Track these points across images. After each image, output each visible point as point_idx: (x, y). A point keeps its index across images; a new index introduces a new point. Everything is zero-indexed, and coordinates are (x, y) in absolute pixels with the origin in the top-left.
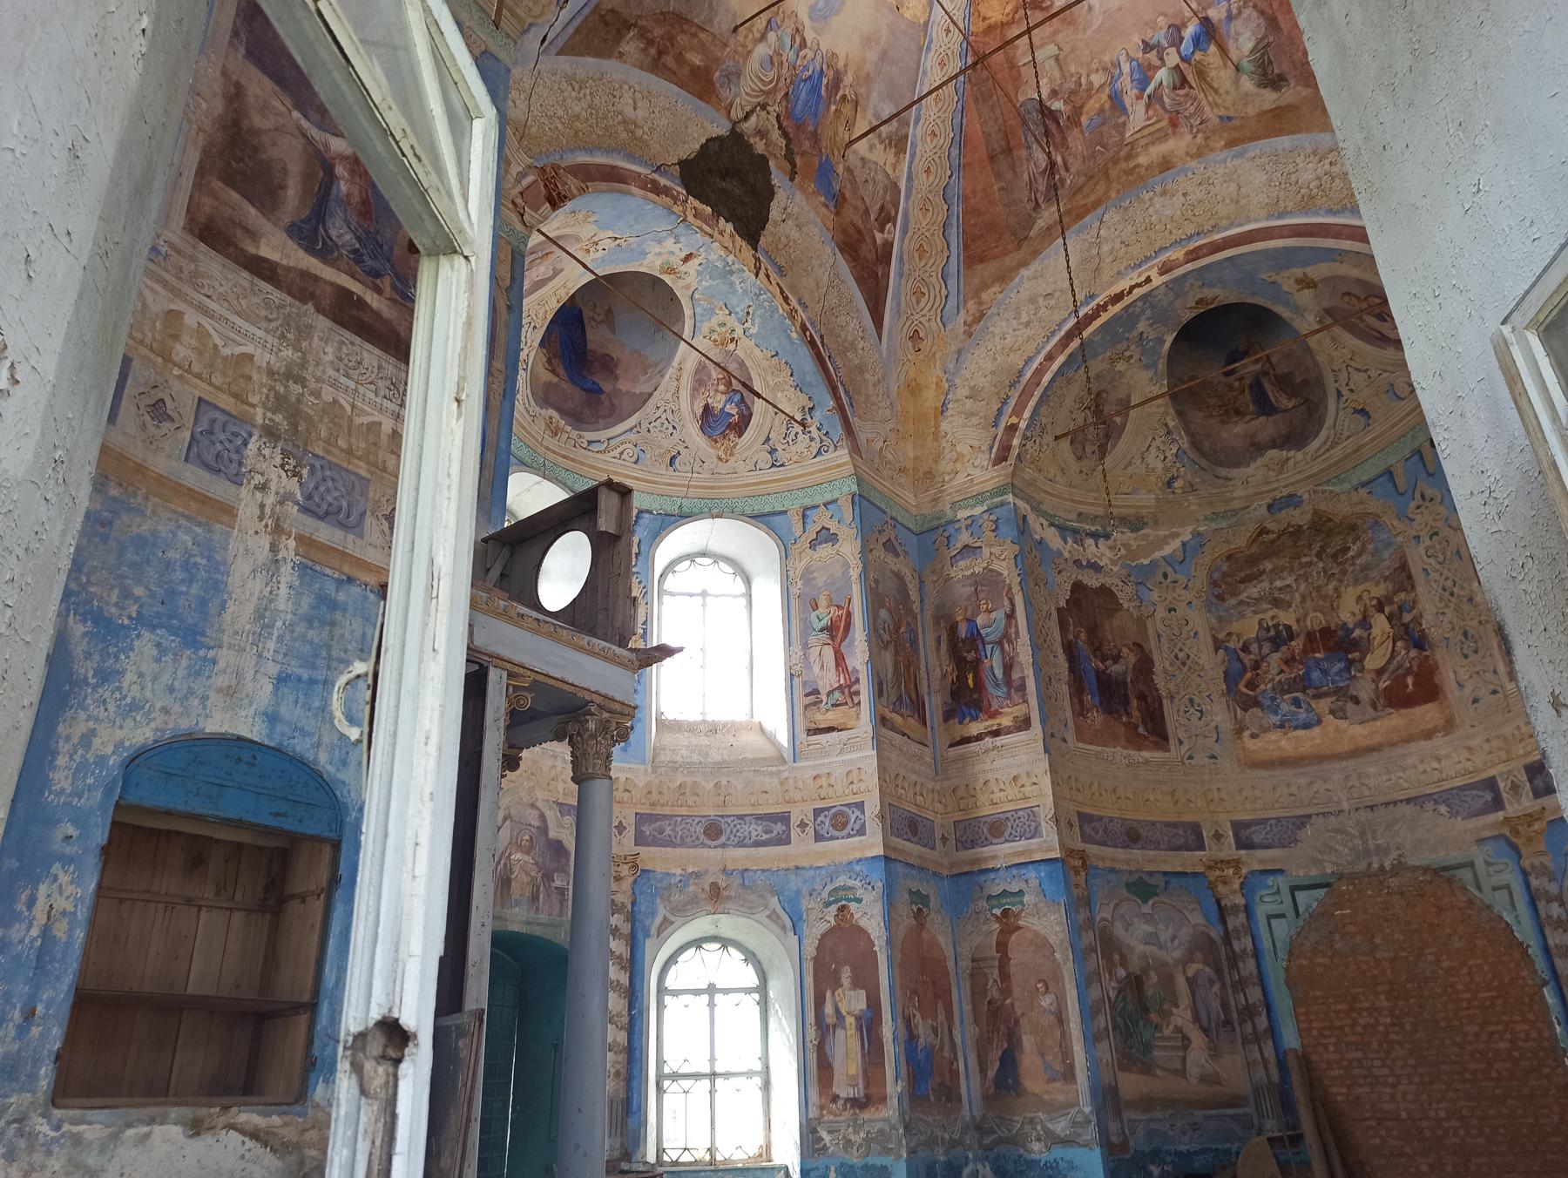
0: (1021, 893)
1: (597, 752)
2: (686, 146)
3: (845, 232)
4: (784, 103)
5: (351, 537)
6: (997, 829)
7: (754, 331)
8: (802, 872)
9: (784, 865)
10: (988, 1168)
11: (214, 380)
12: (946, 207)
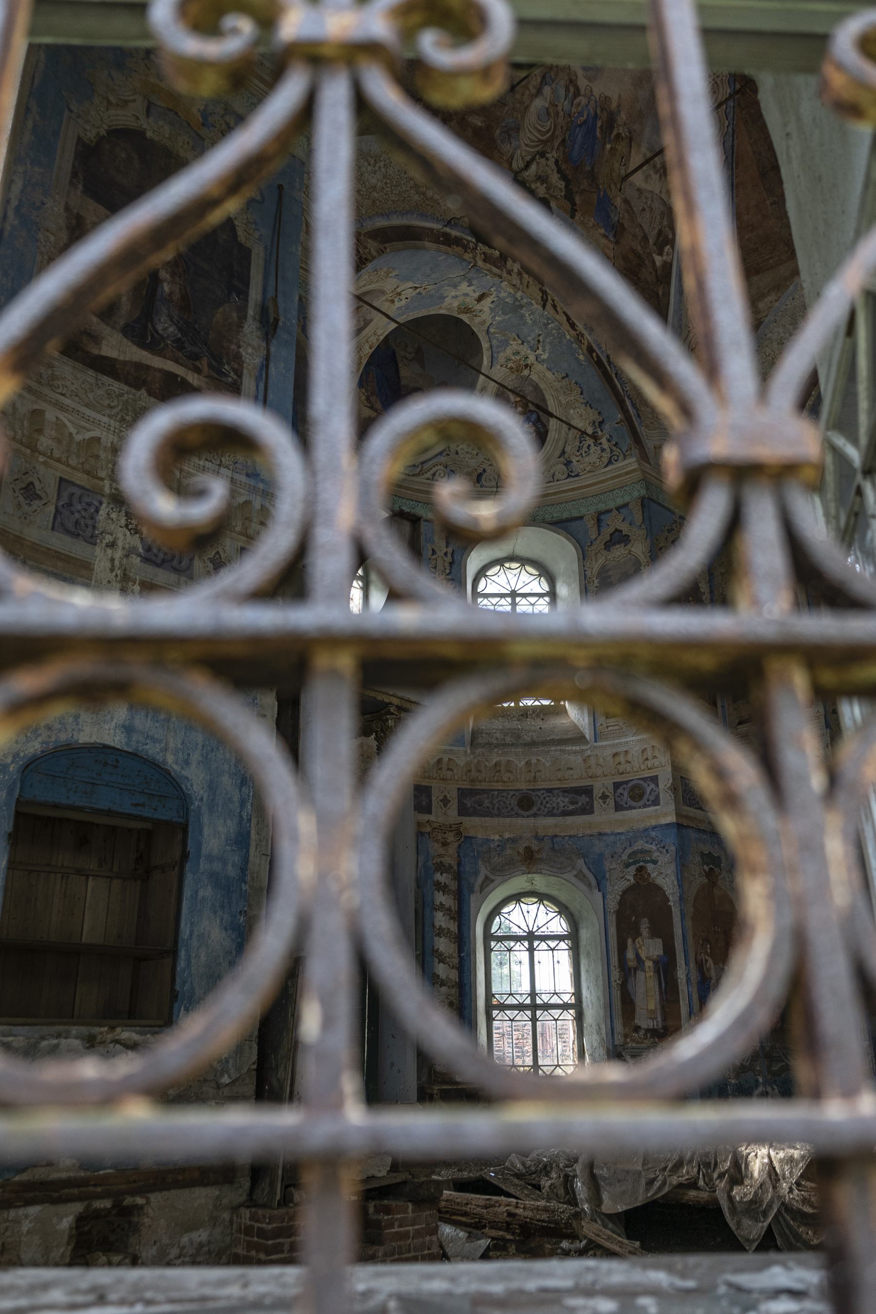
4: (561, 149)
9: (588, 832)
11: (71, 462)
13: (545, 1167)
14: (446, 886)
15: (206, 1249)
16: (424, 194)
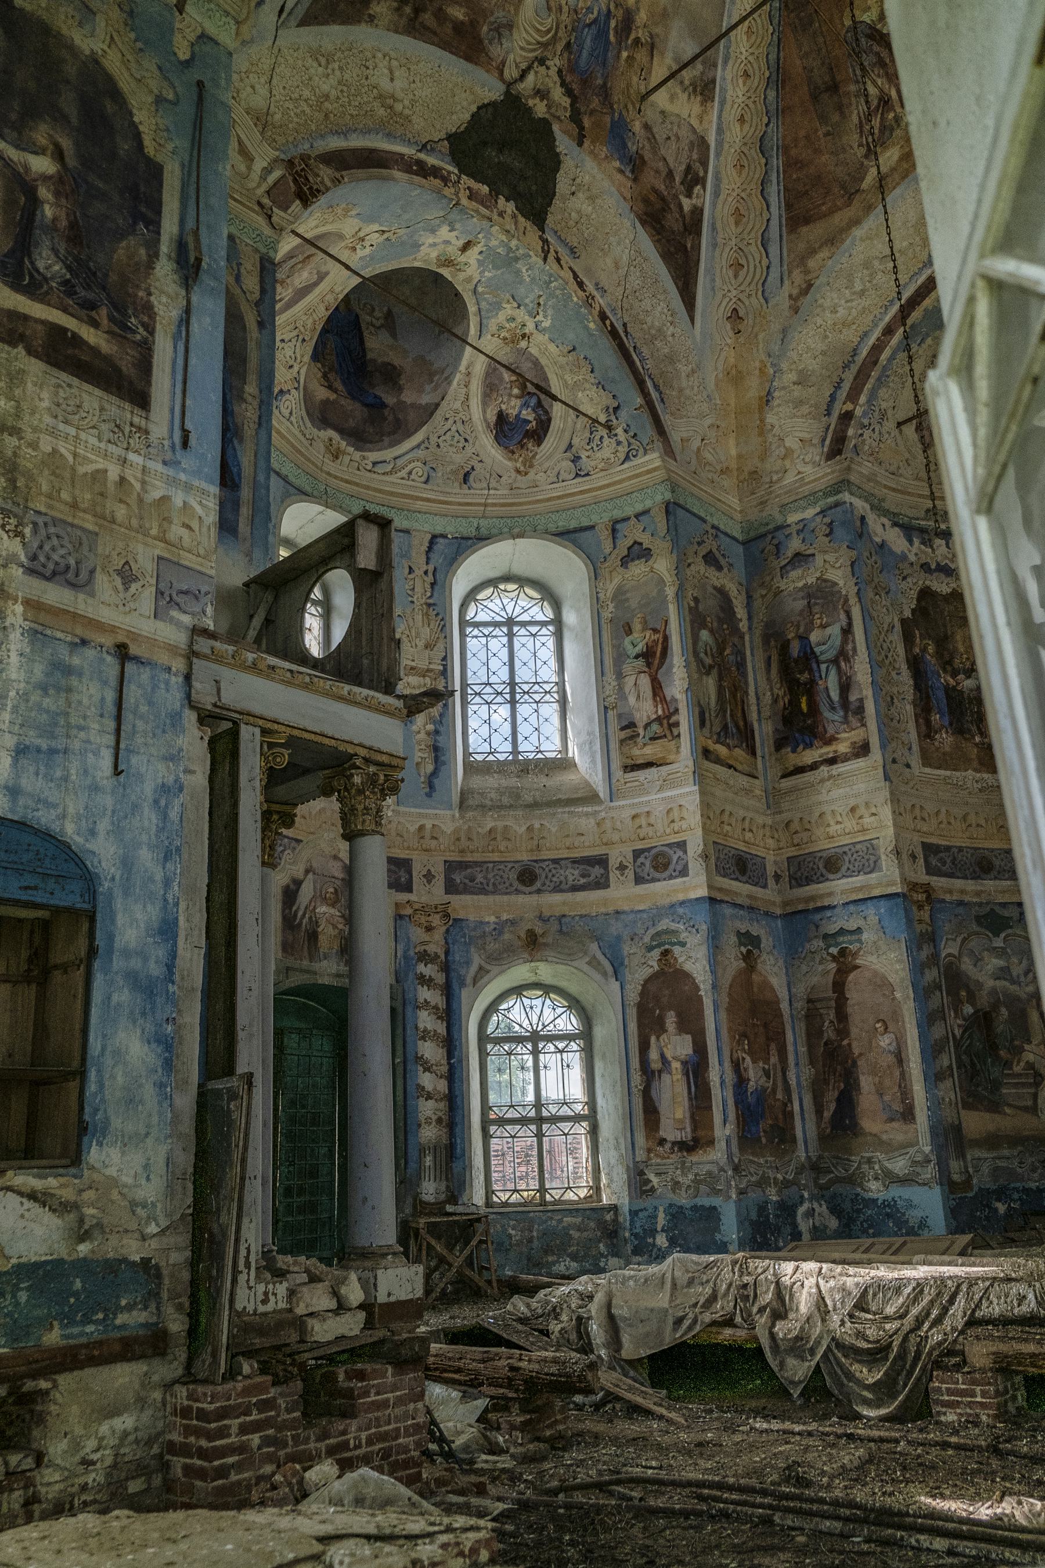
0: (859, 930)
1: (366, 808)
2: (454, 117)
3: (646, 201)
4: (566, 55)
5: (81, 596)
6: (832, 865)
7: (547, 324)
8: (623, 917)
9: (603, 910)
10: (824, 1207)
12: (764, 161)
13: (554, 1309)
14: (431, 979)
15: (131, 1438)
16: (391, 108)
